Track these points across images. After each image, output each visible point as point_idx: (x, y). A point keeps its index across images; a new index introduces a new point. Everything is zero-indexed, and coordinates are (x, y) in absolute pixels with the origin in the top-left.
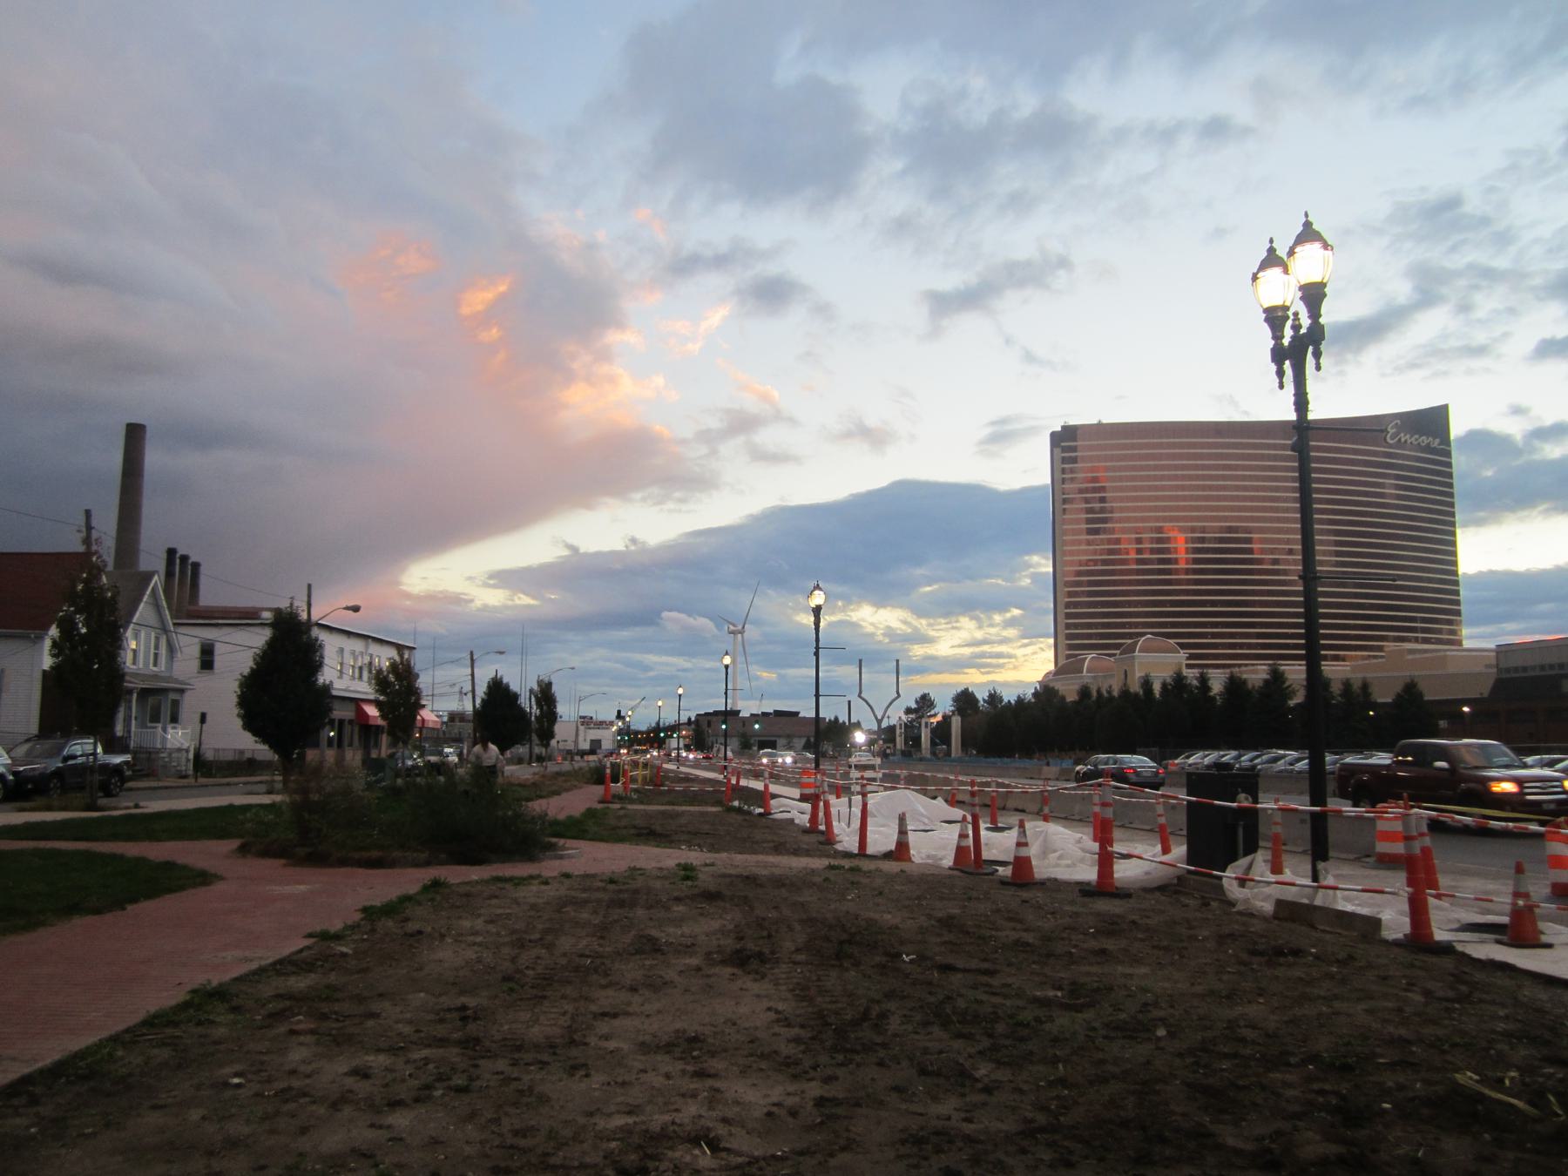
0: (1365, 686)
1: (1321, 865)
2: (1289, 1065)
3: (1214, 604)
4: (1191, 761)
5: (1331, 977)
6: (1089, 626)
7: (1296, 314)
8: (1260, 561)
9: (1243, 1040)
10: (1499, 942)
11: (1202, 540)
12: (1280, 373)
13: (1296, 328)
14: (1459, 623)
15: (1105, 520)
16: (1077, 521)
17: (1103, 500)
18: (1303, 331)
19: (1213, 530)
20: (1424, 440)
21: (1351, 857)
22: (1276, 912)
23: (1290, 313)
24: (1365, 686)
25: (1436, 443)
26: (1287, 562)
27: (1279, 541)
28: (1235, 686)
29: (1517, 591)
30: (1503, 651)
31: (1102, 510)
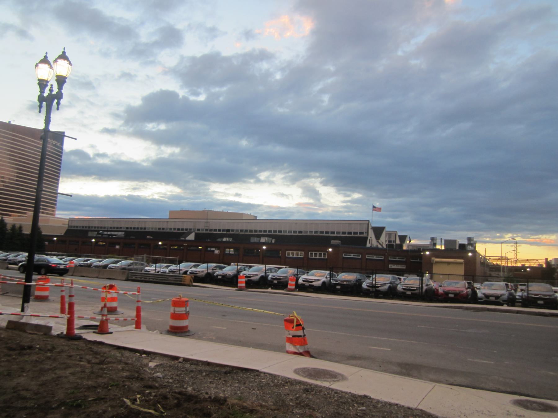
0: (21, 227)
1: (26, 305)
2: (53, 409)
5: (49, 358)
7: (52, 85)
9: (24, 398)
10: (94, 332)
12: (40, 107)
13: (51, 90)
18: (53, 93)
20: (55, 142)
22: (7, 325)
23: (49, 84)
24: (21, 227)
25: (58, 144)
29: (77, 202)
30: (71, 220)
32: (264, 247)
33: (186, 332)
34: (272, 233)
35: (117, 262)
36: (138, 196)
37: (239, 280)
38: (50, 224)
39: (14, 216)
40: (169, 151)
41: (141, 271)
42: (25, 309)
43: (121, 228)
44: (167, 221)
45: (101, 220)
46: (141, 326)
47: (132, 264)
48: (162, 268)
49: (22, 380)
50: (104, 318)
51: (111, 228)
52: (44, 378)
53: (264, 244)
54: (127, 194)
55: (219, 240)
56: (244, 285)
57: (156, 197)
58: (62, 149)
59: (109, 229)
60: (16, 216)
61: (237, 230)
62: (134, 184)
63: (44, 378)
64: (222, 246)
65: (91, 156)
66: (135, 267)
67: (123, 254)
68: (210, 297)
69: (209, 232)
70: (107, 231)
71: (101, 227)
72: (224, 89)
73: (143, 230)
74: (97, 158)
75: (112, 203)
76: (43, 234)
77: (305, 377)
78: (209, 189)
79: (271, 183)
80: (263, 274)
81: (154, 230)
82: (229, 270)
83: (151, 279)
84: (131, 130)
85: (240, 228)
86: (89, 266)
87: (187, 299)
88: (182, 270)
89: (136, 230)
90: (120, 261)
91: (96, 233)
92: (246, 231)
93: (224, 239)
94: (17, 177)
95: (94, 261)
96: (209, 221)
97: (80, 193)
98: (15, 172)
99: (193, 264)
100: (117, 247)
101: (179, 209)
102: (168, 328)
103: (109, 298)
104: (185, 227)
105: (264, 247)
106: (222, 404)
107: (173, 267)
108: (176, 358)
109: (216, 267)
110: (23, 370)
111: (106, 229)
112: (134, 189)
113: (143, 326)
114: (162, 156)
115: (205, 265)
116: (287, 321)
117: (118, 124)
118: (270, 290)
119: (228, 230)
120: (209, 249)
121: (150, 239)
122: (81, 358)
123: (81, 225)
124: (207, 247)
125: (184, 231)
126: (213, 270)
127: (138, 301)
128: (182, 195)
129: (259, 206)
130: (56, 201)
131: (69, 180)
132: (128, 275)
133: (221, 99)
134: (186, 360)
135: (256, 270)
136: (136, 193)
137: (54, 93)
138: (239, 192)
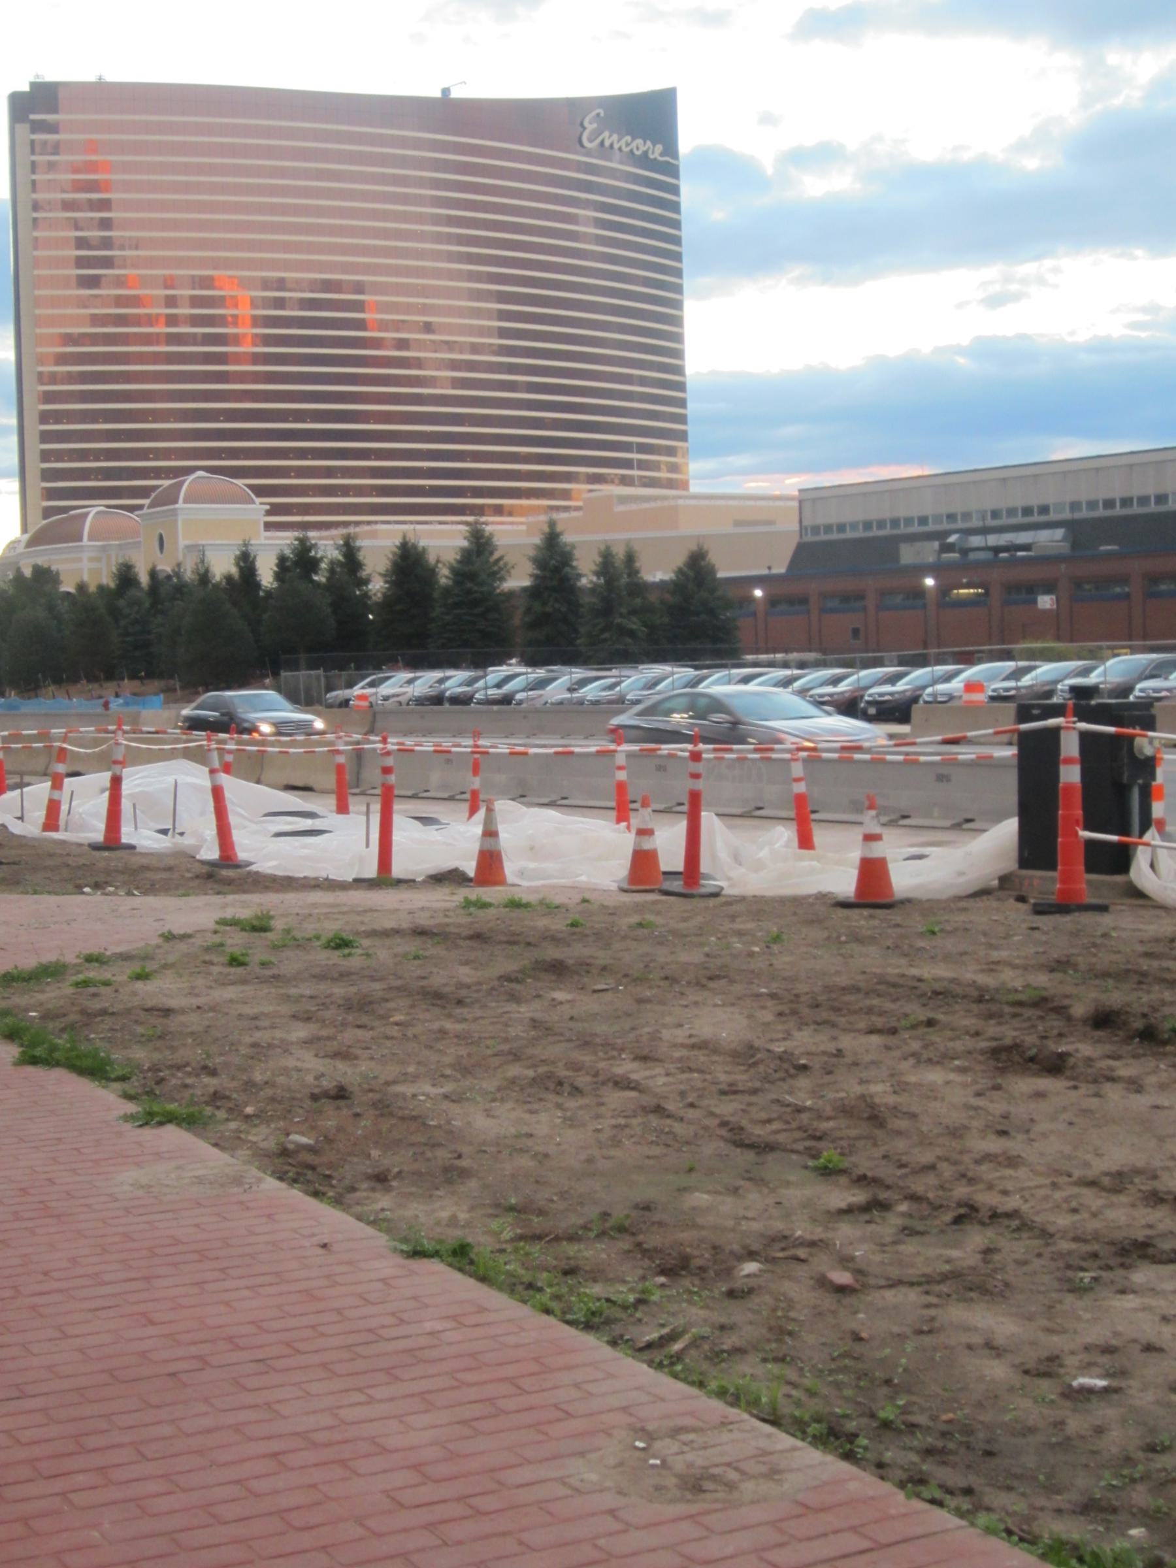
0: (630, 558)
3: (299, 416)
4: (385, 689)
6: (83, 455)
8: (376, 343)
11: (280, 303)
14: (686, 453)
15: (108, 262)
16: (59, 262)
17: (106, 224)
19: (298, 285)
20: (640, 146)
21: (948, 823)
25: (656, 152)
26: (421, 345)
27: (409, 309)
28: (409, 564)
29: (769, 410)
30: (808, 499)
31: (107, 243)
35: (893, 679)
39: (523, 511)
43: (1044, 510)
51: (995, 514)
70: (985, 531)
71: (951, 517)
73: (1153, 508)
76: (720, 575)
89: (1118, 511)
90: (906, 674)
91: (936, 545)
94: (503, 333)
98: (489, 315)
100: (1046, 602)
111: (976, 523)
112: (994, 301)
121: (1109, 556)
123: (860, 516)
130: (682, 419)
136: (1005, 324)
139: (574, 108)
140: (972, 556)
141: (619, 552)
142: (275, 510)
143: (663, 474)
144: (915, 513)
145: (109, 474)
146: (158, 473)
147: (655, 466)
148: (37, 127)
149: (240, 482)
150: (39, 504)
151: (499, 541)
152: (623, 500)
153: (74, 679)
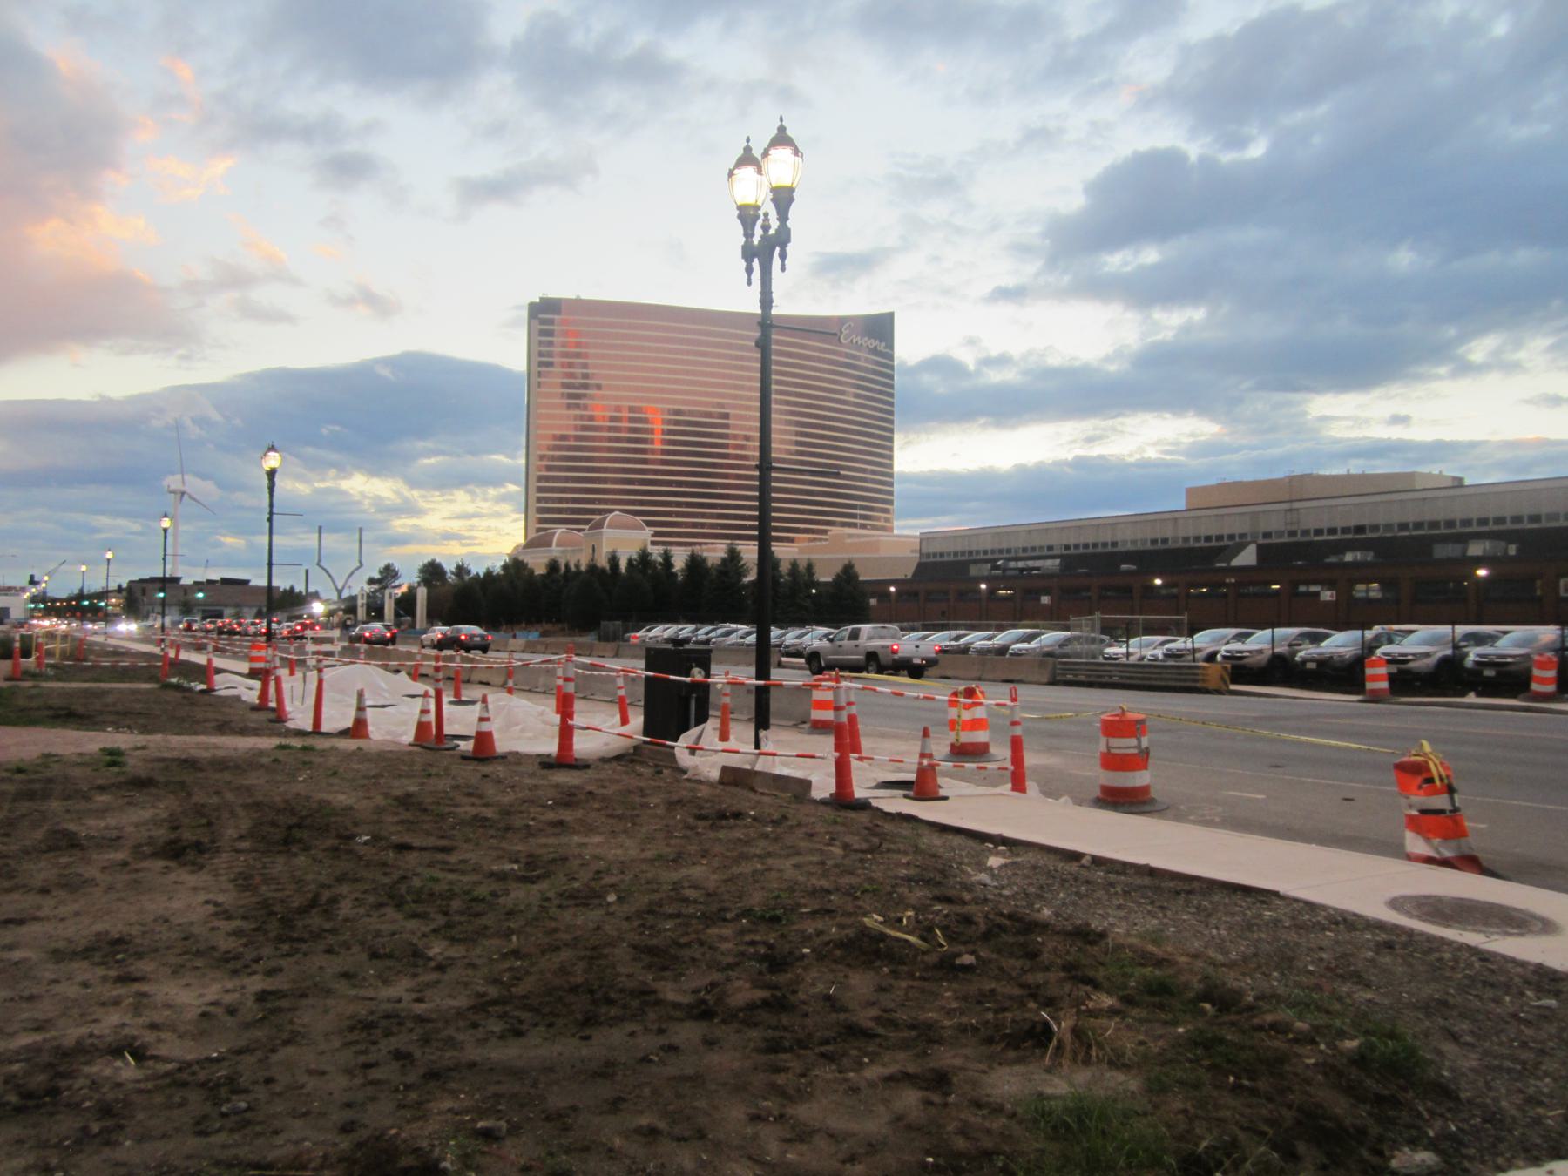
0: (810, 567)
1: (762, 733)
3: (680, 484)
4: (652, 634)
5: (766, 836)
7: (766, 215)
9: (686, 900)
10: (906, 796)
13: (766, 228)
20: (872, 343)
23: (761, 213)
24: (810, 567)
25: (882, 347)
30: (925, 539)
32: (1482, 573)
33: (1144, 803)
34: (1509, 526)
35: (1030, 638)
36: (1101, 457)
37: (1369, 671)
38: (883, 553)
40: (1172, 322)
41: (1094, 657)
42: (762, 744)
44: (1173, 518)
45: (998, 533)
46: (1017, 783)
47: (1067, 641)
48: (1146, 648)
49: (697, 872)
50: (925, 762)
51: (1025, 550)
52: (736, 870)
53: (1479, 561)
54: (1068, 455)
55: (1333, 559)
56: (1384, 685)
57: (1152, 454)
58: (891, 358)
59: (1021, 554)
60: (804, 540)
61: (1388, 527)
62: (1088, 426)
63: (736, 870)
64: (1344, 578)
65: (972, 367)
66: (1078, 648)
67: (1055, 617)
68: (1261, 718)
69: (1299, 538)
70: (1017, 559)
71: (1001, 551)
72: (1322, 109)
74: (985, 370)
75: (1034, 483)
77: (1419, 918)
78: (1305, 413)
79: (1513, 368)
80: (1449, 652)
81: (1139, 547)
82: (1340, 643)
83: (1115, 679)
84: (1067, 279)
85: (1396, 518)
86: (965, 650)
87: (1142, 716)
88: (1200, 650)
89: (1091, 550)
92: (1418, 525)
93: (1349, 557)
95: (976, 639)
96: (1296, 505)
97: (952, 471)
99: (1234, 631)
100: (1045, 600)
101: (1213, 482)
102: (1098, 793)
103: (965, 722)
104: (1226, 532)
105: (1482, 573)
106: (1092, 943)
107: (1180, 643)
108: (1075, 856)
109: (1302, 635)
110: (704, 854)
111: (1013, 555)
112: (1090, 440)
113: (1032, 786)
114: (1160, 337)
115: (1268, 631)
116: (1401, 767)
117: (1030, 269)
118: (1472, 698)
119: (1360, 529)
120: (1302, 588)
122: (832, 839)
124: (1296, 584)
125: (1226, 542)
126: (1290, 645)
127: (1014, 723)
128: (1227, 439)
129: (1473, 445)
130: (891, 493)
131: (923, 437)
132: (1054, 668)
133: (1316, 140)
134: (1098, 861)
135: (1421, 642)
136: (1096, 451)
137: (772, 232)
138: (1403, 412)
139: (842, 321)
140: (1009, 573)
141: (802, 566)
142: (656, 534)
143: (882, 523)
144: (981, 548)
145: (573, 511)
146: (593, 512)
147: (878, 519)
148: (543, 322)
149: (638, 518)
150: (534, 525)
151: (744, 555)
152: (850, 536)
153: (519, 622)
